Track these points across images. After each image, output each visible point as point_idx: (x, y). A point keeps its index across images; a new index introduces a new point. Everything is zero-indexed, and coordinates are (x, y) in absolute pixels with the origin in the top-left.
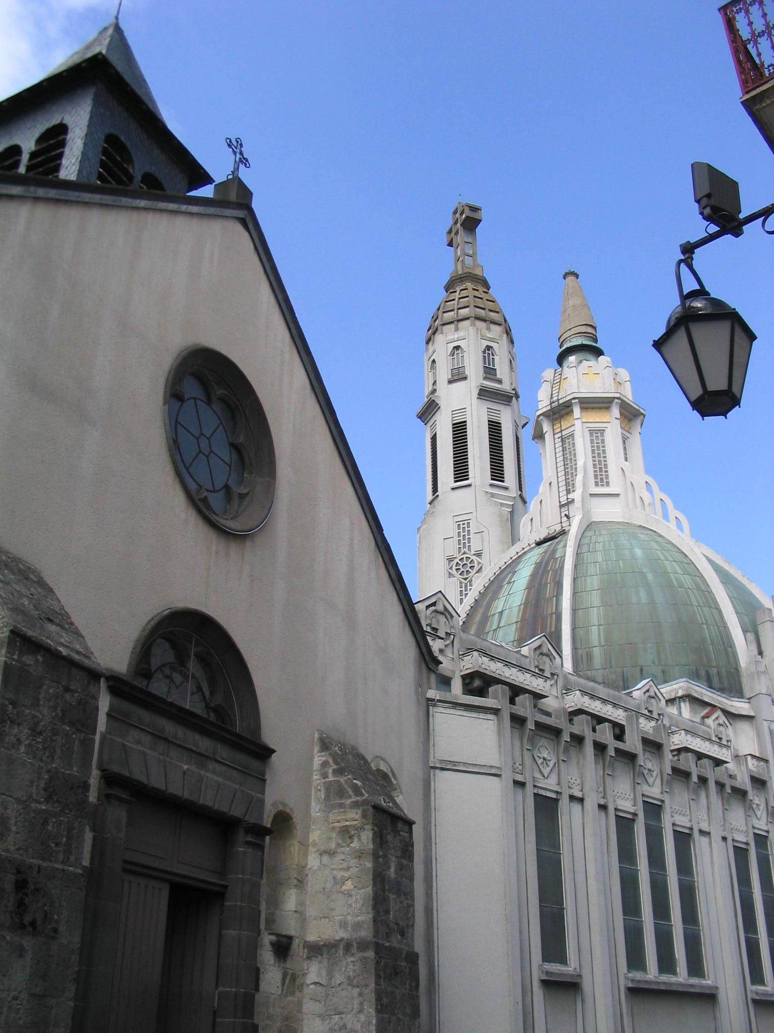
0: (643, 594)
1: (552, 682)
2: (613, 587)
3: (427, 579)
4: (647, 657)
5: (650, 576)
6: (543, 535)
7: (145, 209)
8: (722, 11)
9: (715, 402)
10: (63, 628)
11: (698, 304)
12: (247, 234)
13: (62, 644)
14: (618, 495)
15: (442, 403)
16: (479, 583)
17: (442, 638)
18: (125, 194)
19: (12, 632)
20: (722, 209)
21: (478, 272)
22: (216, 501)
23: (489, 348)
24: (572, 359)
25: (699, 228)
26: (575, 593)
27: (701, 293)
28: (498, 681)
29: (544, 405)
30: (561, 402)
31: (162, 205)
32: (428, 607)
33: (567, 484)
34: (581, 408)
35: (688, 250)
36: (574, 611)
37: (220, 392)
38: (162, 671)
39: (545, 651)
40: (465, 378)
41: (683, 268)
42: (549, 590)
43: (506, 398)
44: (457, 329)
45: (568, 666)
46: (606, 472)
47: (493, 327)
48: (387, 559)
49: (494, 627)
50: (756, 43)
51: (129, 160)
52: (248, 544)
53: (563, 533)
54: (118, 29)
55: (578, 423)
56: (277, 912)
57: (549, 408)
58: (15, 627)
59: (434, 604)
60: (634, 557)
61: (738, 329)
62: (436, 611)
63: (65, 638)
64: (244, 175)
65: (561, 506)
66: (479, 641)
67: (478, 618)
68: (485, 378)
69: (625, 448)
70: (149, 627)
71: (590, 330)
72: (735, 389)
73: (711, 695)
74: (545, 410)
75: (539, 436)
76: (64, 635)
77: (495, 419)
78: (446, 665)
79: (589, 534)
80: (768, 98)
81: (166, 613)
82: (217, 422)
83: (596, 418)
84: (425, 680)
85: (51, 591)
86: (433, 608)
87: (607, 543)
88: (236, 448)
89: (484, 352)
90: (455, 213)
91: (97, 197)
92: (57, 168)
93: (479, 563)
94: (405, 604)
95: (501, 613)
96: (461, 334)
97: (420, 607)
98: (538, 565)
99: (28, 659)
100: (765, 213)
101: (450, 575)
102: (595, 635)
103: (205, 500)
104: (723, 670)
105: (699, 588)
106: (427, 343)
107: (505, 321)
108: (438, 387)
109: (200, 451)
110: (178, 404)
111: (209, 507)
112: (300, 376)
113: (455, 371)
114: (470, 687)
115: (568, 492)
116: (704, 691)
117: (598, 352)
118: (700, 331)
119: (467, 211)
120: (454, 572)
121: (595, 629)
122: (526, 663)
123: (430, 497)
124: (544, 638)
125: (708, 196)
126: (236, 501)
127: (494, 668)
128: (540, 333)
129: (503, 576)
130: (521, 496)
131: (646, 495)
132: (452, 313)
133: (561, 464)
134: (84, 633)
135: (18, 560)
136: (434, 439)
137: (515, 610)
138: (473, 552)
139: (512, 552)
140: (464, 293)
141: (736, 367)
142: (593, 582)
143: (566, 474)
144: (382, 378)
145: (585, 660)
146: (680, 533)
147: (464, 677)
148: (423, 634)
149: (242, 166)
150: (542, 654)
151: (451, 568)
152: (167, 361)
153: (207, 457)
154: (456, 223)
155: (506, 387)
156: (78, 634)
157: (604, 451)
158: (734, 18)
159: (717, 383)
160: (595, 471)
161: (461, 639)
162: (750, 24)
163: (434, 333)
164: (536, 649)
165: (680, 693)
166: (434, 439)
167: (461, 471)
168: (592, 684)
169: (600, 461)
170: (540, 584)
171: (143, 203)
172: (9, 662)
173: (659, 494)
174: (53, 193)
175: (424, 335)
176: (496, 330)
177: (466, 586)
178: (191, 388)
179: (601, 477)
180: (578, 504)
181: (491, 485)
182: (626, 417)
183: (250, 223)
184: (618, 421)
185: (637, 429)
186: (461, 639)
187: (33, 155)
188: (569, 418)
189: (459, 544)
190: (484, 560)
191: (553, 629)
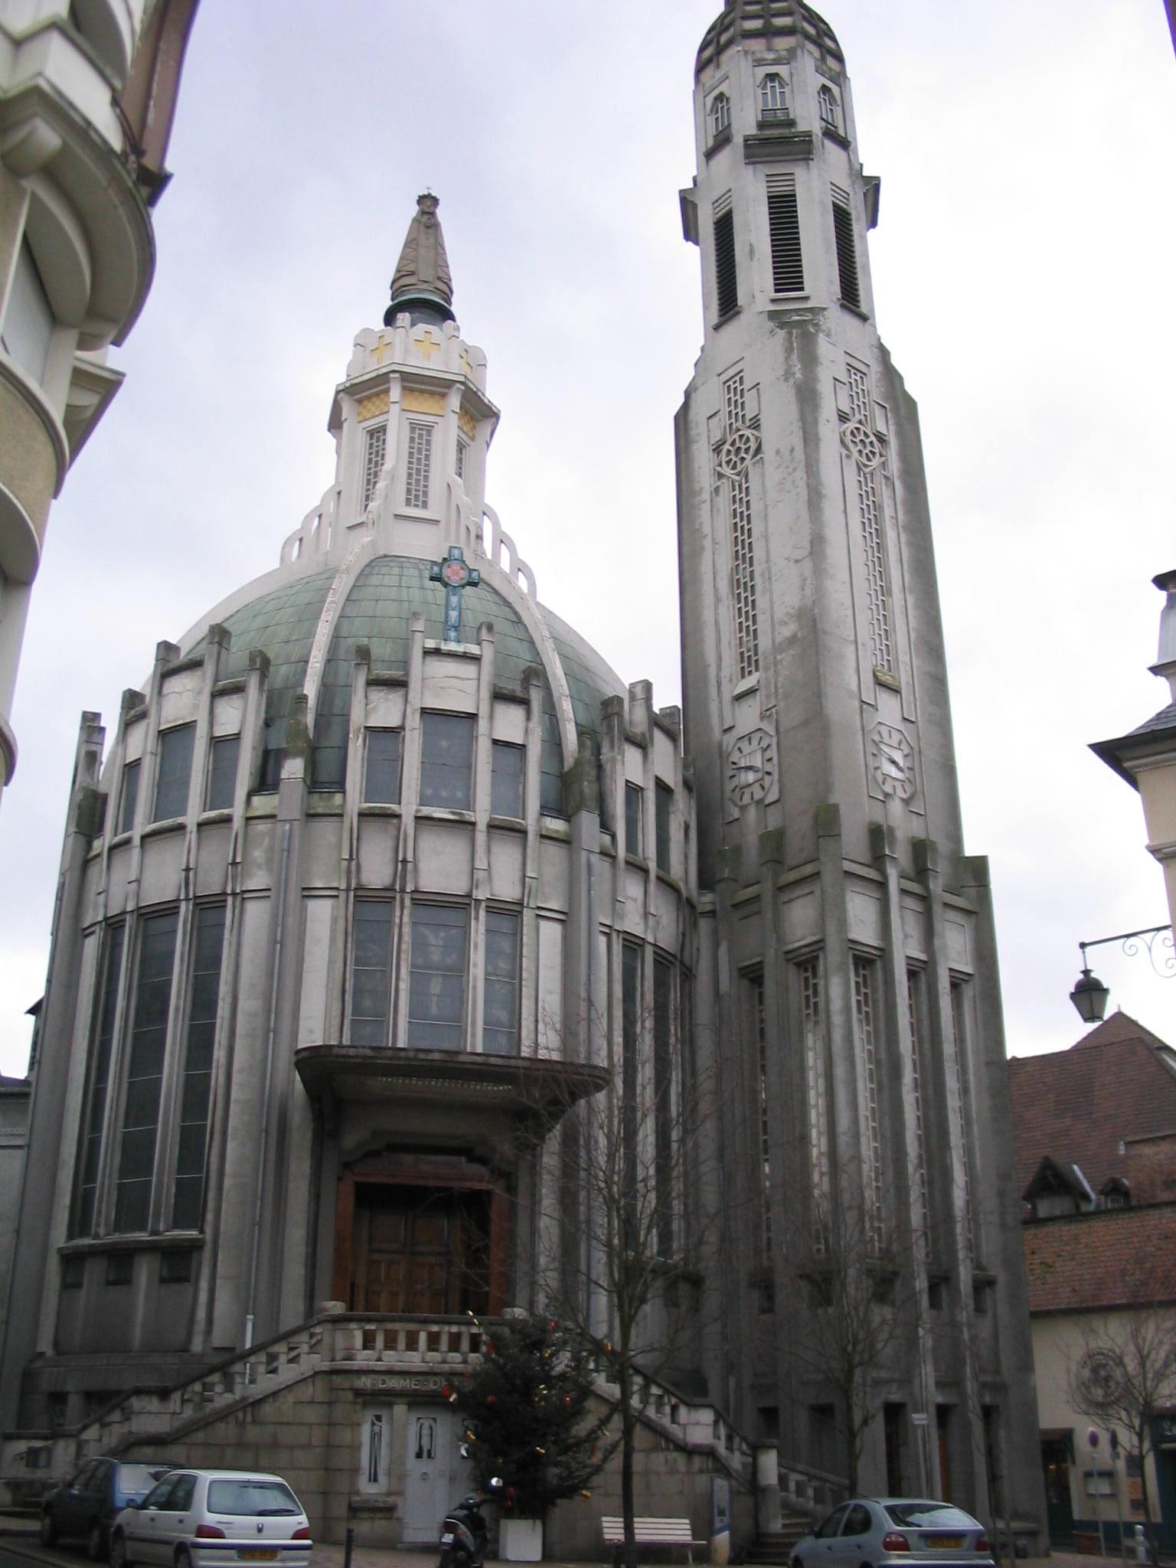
34: (404, 388)
44: (718, 66)
46: (426, 486)
55: (395, 409)
56: (988, 1291)
69: (460, 460)
83: (423, 408)
169: (418, 470)
179: (417, 495)
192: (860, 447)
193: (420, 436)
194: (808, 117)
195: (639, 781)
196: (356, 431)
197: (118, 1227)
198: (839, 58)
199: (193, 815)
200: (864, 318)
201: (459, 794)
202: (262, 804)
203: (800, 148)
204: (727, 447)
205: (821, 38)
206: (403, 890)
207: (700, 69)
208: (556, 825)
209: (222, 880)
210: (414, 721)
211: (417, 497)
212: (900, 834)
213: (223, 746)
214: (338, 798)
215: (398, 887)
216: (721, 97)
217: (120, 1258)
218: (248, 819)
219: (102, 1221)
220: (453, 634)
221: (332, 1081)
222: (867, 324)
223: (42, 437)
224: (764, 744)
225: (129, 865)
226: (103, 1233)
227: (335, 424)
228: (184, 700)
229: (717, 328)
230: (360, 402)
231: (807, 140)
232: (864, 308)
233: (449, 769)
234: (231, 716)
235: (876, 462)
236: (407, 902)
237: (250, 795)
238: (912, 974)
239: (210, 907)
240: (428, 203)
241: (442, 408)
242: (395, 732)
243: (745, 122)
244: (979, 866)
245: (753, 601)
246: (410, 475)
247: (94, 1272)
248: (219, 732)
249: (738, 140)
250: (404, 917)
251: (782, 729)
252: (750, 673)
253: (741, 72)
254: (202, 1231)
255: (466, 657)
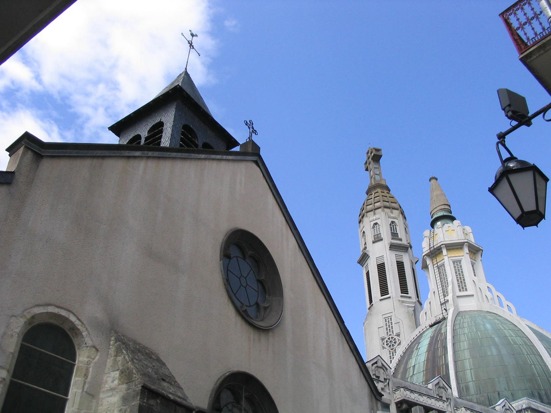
0: (494, 350)
1: (448, 403)
2: (476, 347)
3: (371, 349)
4: (501, 386)
5: (497, 339)
6: (433, 321)
7: (205, 159)
8: (501, 16)
9: (530, 218)
10: (171, 384)
11: (511, 165)
12: (258, 169)
13: (170, 393)
14: (473, 295)
15: (370, 254)
16: (400, 351)
17: (382, 382)
18: (193, 152)
19: (143, 387)
20: (518, 113)
21: (383, 183)
22: (252, 311)
23: (393, 222)
24: (439, 223)
25: (506, 124)
26: (454, 352)
27: (512, 158)
28: (416, 404)
29: (426, 250)
30: (435, 247)
31: (213, 156)
32: (373, 365)
33: (443, 292)
34: (447, 250)
35: (502, 137)
36: (455, 362)
37: (250, 252)
38: (227, 407)
39: (441, 385)
40: (382, 240)
41: (500, 145)
42: (440, 352)
43: (405, 248)
44: (375, 214)
45: (455, 394)
46: (465, 283)
47: (394, 211)
48: (348, 338)
49: (411, 374)
50: (523, 28)
51: (196, 137)
52: (271, 334)
53: (444, 319)
54: (186, 73)
55: (446, 258)
57: (429, 251)
58: (144, 384)
59: (376, 363)
60: (486, 329)
61: (538, 178)
62: (377, 367)
63: (172, 390)
64: (255, 138)
65: (441, 304)
66: (403, 382)
67: (401, 370)
68: (392, 239)
70: (219, 382)
71: (447, 207)
72: (541, 209)
73: (543, 407)
74: (427, 252)
75: (425, 267)
76: (172, 388)
77: (400, 260)
78: (386, 397)
79: (459, 318)
80: (534, 55)
81: (227, 374)
82: (251, 271)
83: (456, 255)
84: (375, 405)
85: (164, 364)
86: (375, 365)
87: (470, 323)
88: (260, 282)
89: (391, 225)
90: (368, 153)
91: (179, 155)
92: (159, 143)
93: (399, 340)
94: (360, 363)
95: (414, 366)
96: (377, 216)
97: (368, 365)
98: (432, 338)
99: (152, 402)
100: (544, 111)
101: (383, 348)
102: (469, 375)
103: (245, 311)
104: (549, 391)
105: (526, 344)
106: (360, 223)
107: (400, 207)
108: (367, 246)
109: (241, 285)
110: (228, 260)
111: (248, 315)
112: (293, 241)
113: (376, 236)
114: (400, 409)
115: (445, 296)
116: (539, 405)
117: (452, 219)
118: (513, 178)
119: (374, 151)
120: (385, 346)
121: (468, 372)
122: (431, 393)
123: (368, 305)
124: (440, 378)
125: (509, 105)
126: (262, 310)
127: (413, 397)
128: (420, 209)
129: (412, 346)
130: (418, 301)
131: (488, 294)
132: (371, 206)
133: (439, 281)
134: (183, 387)
135: (145, 348)
136: (368, 274)
137: (422, 364)
138: (395, 334)
139: (417, 332)
140: (377, 195)
141: (539, 198)
142: (464, 345)
143: (442, 286)
144: (337, 239)
145: (465, 390)
146: (510, 313)
147: (397, 404)
148: (372, 380)
149: (253, 134)
150: (440, 387)
151: (384, 344)
152: (221, 238)
153: (245, 288)
154: (369, 158)
155: (404, 242)
156: (179, 387)
157: (462, 272)
158: (508, 18)
159: (530, 206)
160: (458, 283)
161: (393, 381)
162: (518, 19)
163: (363, 217)
164: (436, 385)
165: (524, 407)
166: (368, 274)
167: (384, 290)
168: (471, 403)
169: (460, 278)
170: (434, 349)
171: (203, 156)
172: (142, 404)
173: (496, 293)
174: (156, 154)
175: (357, 219)
176: (396, 213)
177: (393, 353)
178: (234, 252)
179: (462, 286)
180: (451, 302)
181: (401, 296)
182: (472, 252)
183: (260, 163)
184: (468, 255)
185: (479, 258)
186: (393, 381)
187: (147, 139)
188: (440, 255)
189: (387, 330)
190: (402, 338)
191: (445, 374)
193: (457, 264)
211: (463, 288)
223: (268, 326)
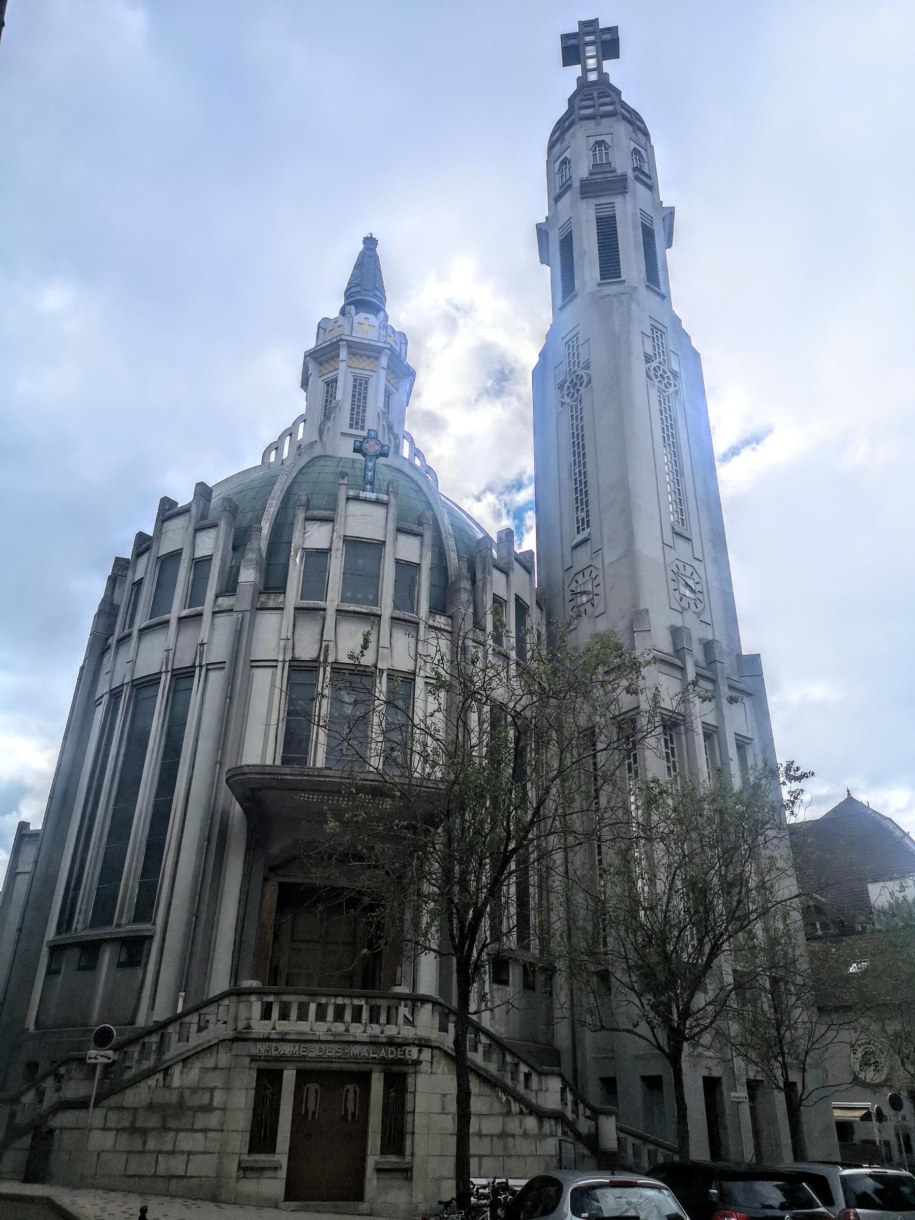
34: (349, 353)
55: (342, 366)
83: (363, 367)
192: (660, 379)
194: (622, 164)
195: (502, 593)
196: (318, 384)
197: (93, 925)
198: (646, 134)
199: (177, 610)
200: (663, 297)
201: (371, 597)
202: (224, 602)
203: (619, 186)
204: (567, 384)
205: (634, 121)
206: (325, 661)
207: (551, 147)
208: (441, 621)
209: (193, 656)
210: (339, 544)
211: (357, 423)
212: (694, 637)
213: (201, 564)
214: (281, 599)
215: (321, 659)
216: (566, 162)
217: (90, 950)
218: (214, 613)
219: (81, 920)
220: (369, 487)
221: (260, 800)
222: (666, 301)
224: (593, 576)
225: (127, 652)
226: (81, 927)
227: (305, 384)
228: (175, 536)
229: (561, 309)
230: (321, 364)
231: (624, 178)
232: (663, 290)
233: (361, 580)
234: (208, 544)
235: (671, 389)
236: (329, 669)
237: (217, 597)
238: (707, 736)
239: (182, 677)
240: (575, 547)
241: (376, 366)
242: (324, 553)
243: (582, 170)
244: (755, 659)
245: (587, 501)
246: (352, 409)
247: (71, 959)
248: (199, 554)
249: (576, 184)
250: (324, 676)
251: (606, 564)
252: (583, 529)
253: (580, 141)
254: (154, 924)
255: (377, 502)
